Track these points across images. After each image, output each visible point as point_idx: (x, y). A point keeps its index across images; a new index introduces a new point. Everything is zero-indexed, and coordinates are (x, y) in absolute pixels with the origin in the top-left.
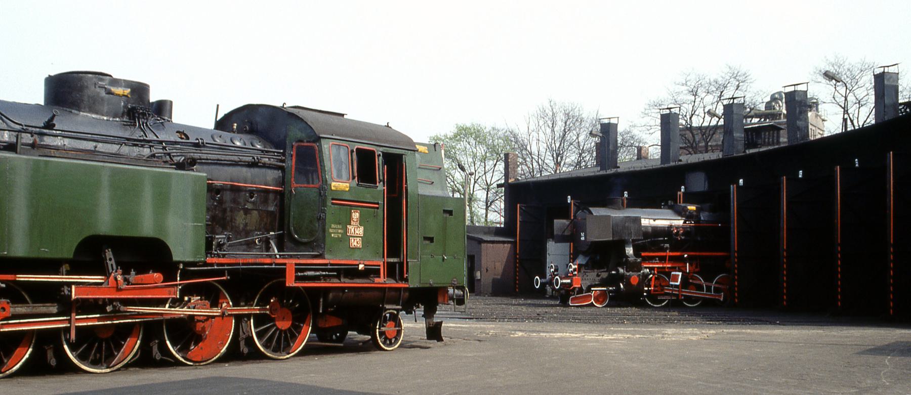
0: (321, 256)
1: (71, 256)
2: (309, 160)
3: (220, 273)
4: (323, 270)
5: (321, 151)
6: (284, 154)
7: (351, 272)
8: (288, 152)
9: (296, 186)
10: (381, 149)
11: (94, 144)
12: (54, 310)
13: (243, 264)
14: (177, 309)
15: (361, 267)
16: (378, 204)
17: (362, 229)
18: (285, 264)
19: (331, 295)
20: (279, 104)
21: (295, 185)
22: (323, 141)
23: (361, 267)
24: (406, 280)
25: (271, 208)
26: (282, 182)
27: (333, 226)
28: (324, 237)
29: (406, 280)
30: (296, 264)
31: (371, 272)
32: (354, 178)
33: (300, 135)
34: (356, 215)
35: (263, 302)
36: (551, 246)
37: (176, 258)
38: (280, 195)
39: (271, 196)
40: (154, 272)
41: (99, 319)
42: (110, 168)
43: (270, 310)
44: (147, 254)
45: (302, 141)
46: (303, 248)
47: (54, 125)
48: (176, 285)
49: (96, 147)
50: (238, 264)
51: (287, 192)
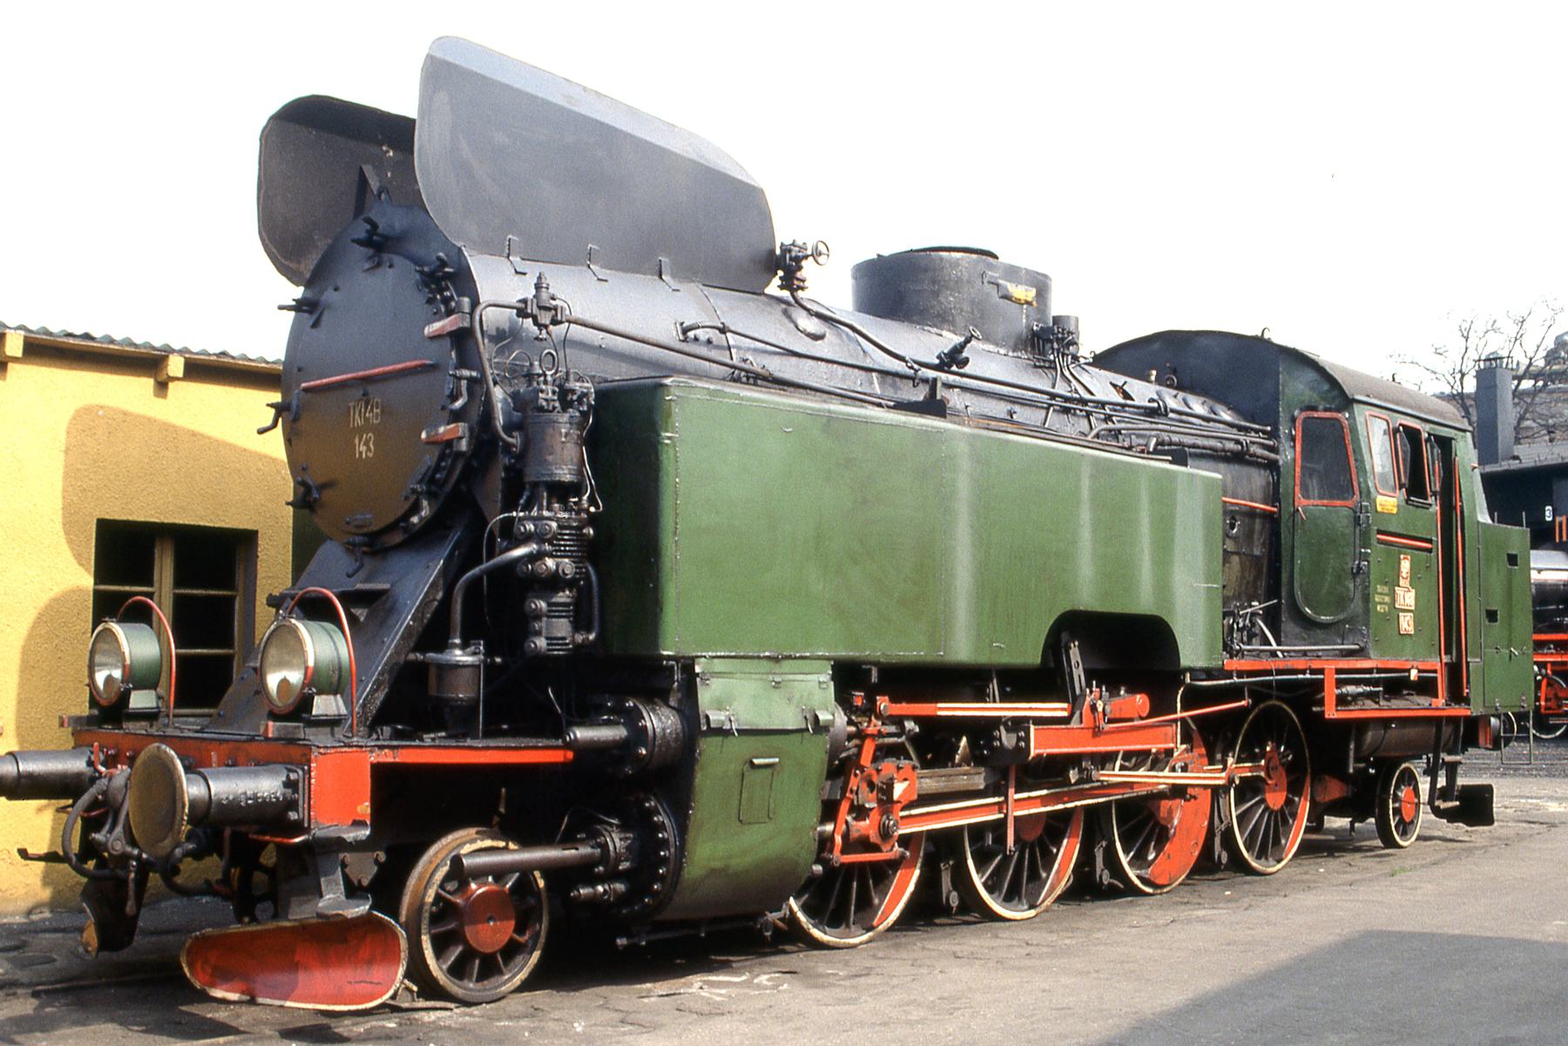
0: (1361, 653)
1: (1038, 660)
2: (1331, 451)
3: (1234, 693)
4: (1357, 682)
5: (1354, 430)
6: (1273, 435)
7: (1396, 686)
8: (1283, 430)
9: (1307, 504)
10: (1428, 427)
11: (1009, 406)
12: (979, 782)
13: (1279, 672)
14: (1141, 772)
15: (1414, 674)
16: (1430, 541)
17: (1413, 593)
18: (1321, 671)
19: (1369, 736)
20: (1250, 330)
21: (1304, 502)
22: (1356, 407)
23: (1414, 674)
24: (1467, 701)
25: (1257, 552)
26: (1274, 495)
27: (1379, 588)
28: (1367, 611)
29: (1467, 701)
30: (1339, 671)
31: (1426, 686)
32: (1401, 487)
33: (1308, 395)
34: (1405, 566)
35: (1248, 755)
36: (1411, 630)
37: (1186, 660)
38: (1272, 520)
39: (1258, 524)
40: (1132, 690)
41: (1044, 800)
42: (1092, 456)
43: (1267, 769)
44: (1128, 649)
45: (1314, 409)
46: (1320, 633)
47: (966, 361)
48: (1175, 721)
49: (1011, 414)
50: (1269, 673)
51: (1285, 516)
